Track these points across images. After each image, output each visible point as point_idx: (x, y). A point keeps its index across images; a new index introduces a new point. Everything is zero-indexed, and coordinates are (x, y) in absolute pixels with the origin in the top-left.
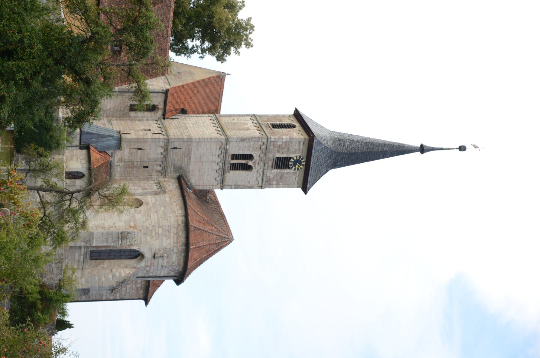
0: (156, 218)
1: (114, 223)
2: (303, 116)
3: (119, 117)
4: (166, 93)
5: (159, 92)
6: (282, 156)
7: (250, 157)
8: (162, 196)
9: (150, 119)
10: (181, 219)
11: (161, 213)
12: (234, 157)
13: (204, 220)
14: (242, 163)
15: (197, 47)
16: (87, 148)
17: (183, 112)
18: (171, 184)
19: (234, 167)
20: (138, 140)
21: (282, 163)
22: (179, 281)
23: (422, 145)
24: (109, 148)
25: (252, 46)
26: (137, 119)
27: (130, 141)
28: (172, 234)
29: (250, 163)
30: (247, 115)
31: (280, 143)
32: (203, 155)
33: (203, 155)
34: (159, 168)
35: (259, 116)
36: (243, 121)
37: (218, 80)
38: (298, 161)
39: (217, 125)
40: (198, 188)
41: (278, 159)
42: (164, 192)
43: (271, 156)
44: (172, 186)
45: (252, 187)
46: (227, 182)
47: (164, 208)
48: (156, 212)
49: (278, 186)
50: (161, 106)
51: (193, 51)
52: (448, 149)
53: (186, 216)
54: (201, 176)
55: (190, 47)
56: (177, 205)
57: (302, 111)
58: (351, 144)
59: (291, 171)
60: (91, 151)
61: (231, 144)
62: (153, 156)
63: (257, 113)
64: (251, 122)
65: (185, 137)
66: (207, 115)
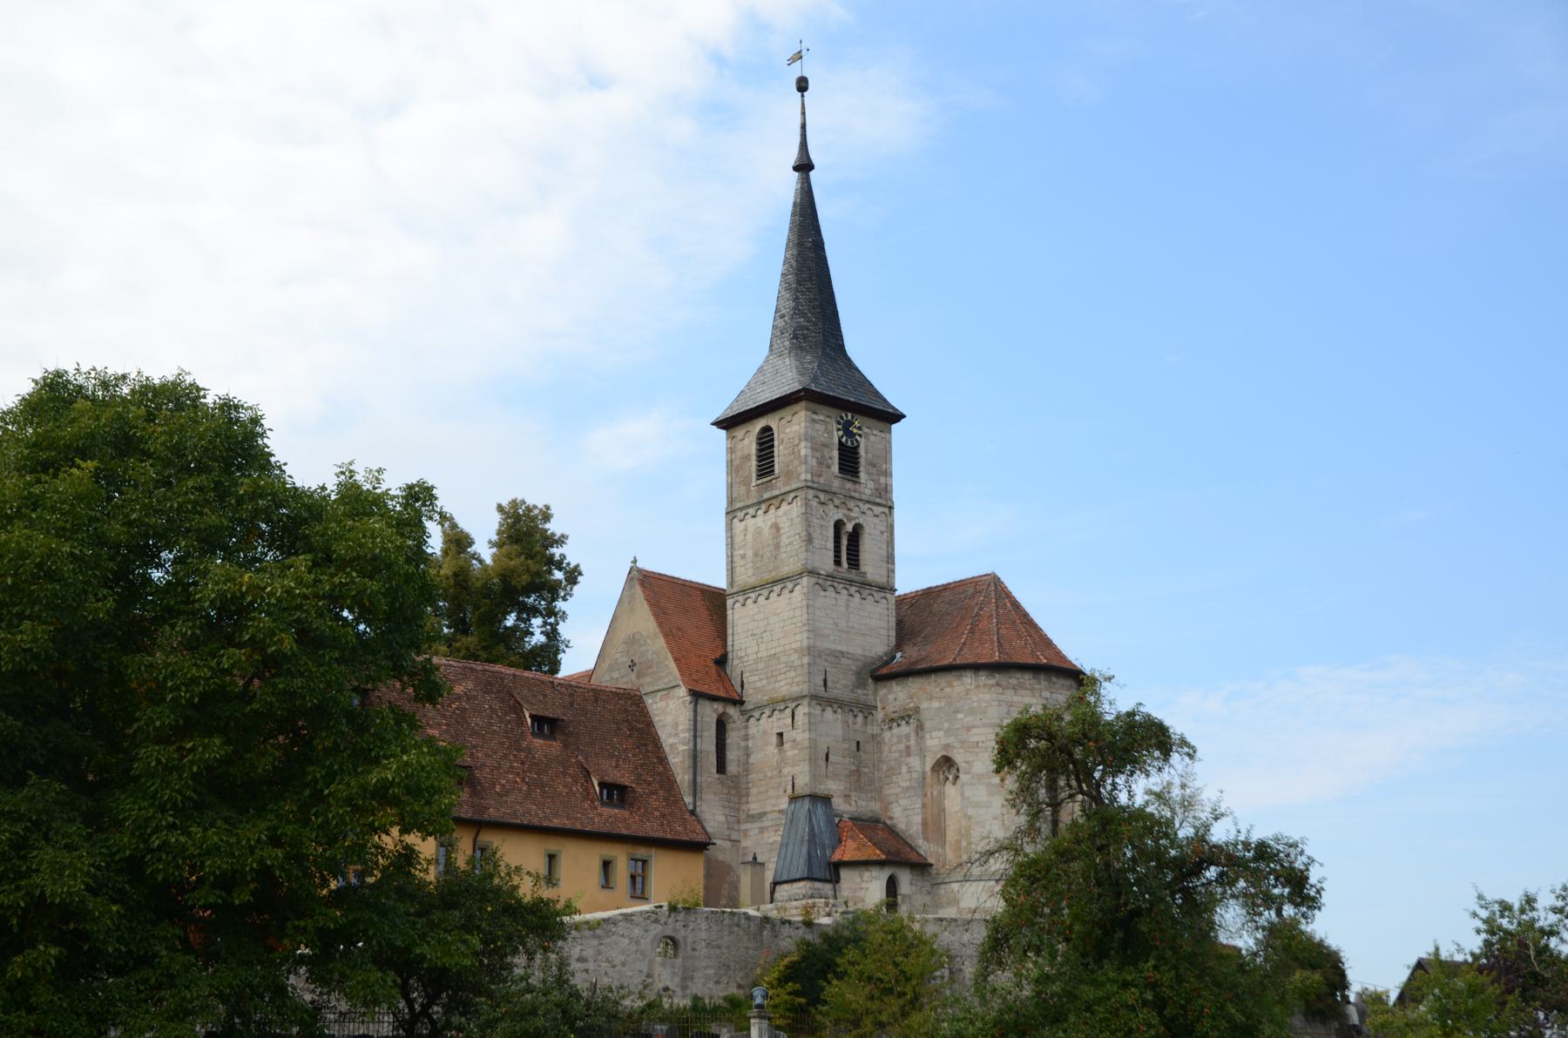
0: (982, 730)
1: (995, 818)
3: (740, 797)
4: (696, 696)
5: (695, 711)
6: (836, 460)
7: (838, 525)
8: (925, 715)
9: (743, 732)
10: (983, 678)
11: (969, 720)
12: (838, 562)
13: (972, 631)
14: (849, 544)
15: (545, 624)
16: (837, 867)
17: (722, 661)
18: (891, 697)
19: (854, 562)
20: (812, 761)
21: (849, 461)
23: (796, 169)
24: (830, 821)
25: (548, 508)
26: (743, 759)
27: (814, 777)
28: (1016, 699)
29: (849, 527)
30: (730, 528)
31: (814, 462)
32: (836, 624)
33: (836, 624)
34: (860, 718)
35: (731, 501)
36: (749, 536)
37: (651, 587)
38: (846, 428)
39: (765, 592)
40: (893, 640)
41: (841, 470)
42: (917, 710)
43: (836, 484)
44: (897, 695)
45: (891, 528)
46: (882, 580)
48: (969, 729)
49: (887, 474)
50: (719, 707)
51: (552, 635)
52: (803, 113)
53: (976, 668)
54: (870, 628)
55: (543, 639)
57: (721, 410)
58: (803, 315)
59: (863, 442)
60: (846, 858)
61: (817, 564)
62: (838, 730)
63: (722, 504)
64: (750, 521)
65: (806, 660)
66: (729, 612)
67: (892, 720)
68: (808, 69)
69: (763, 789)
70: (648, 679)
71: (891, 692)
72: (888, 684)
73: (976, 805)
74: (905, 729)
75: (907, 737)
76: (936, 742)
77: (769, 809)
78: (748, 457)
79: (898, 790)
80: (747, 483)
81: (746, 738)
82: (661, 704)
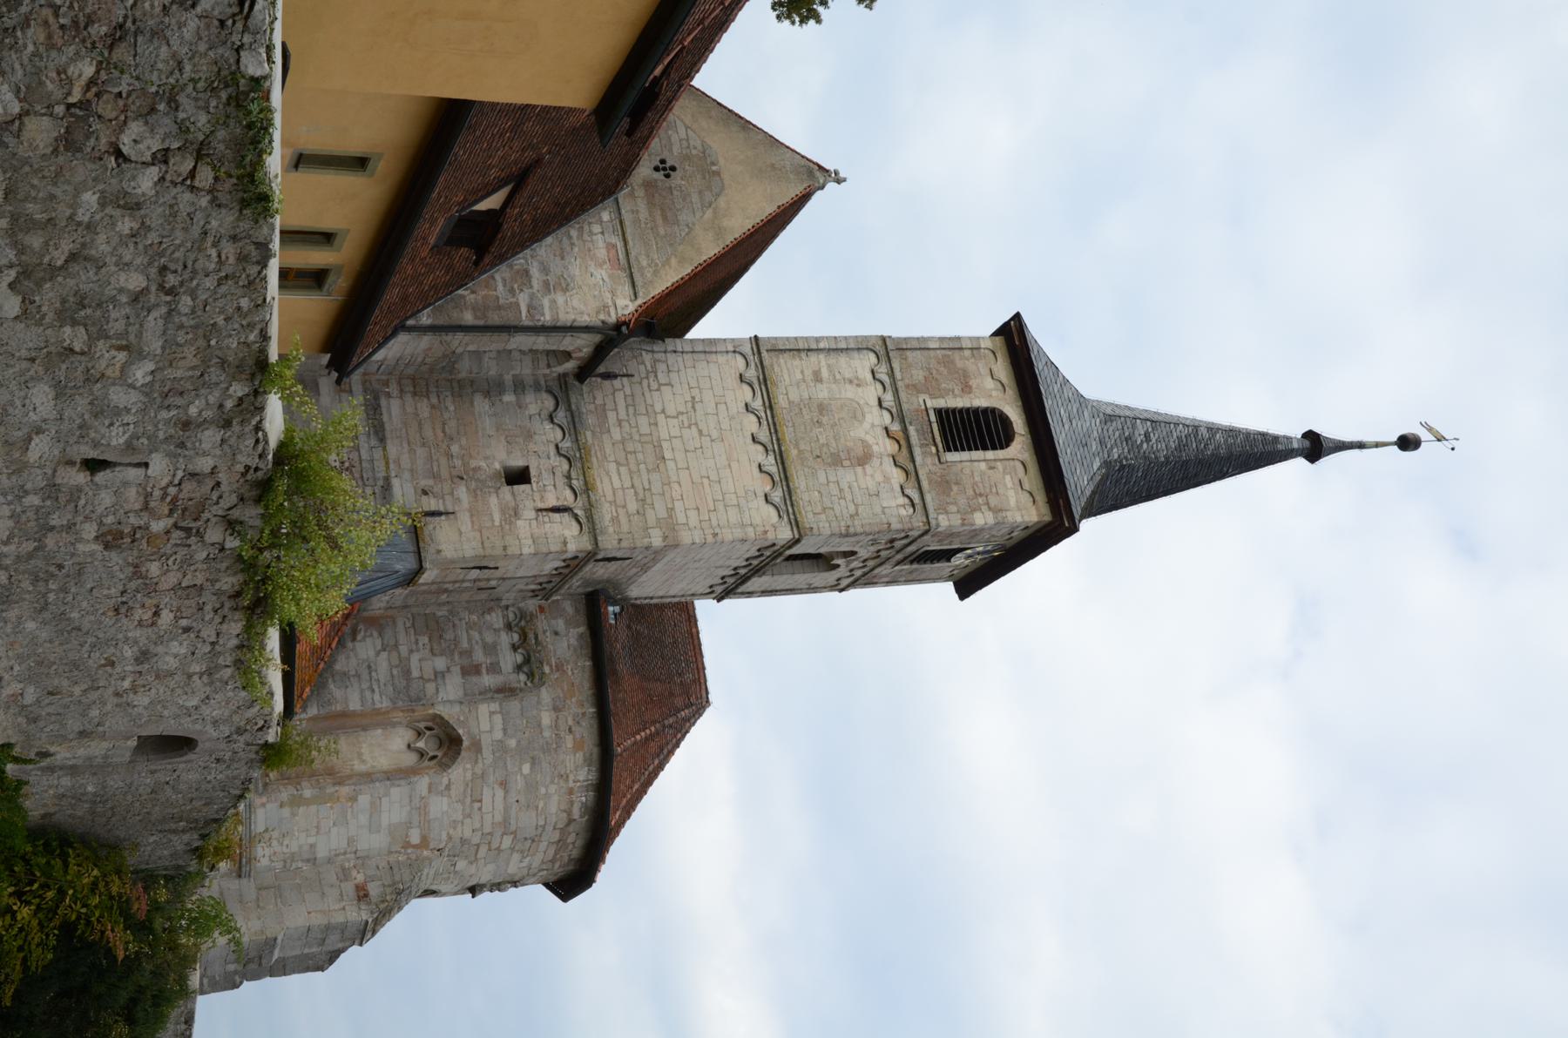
0: (499, 805)
1: (350, 841)
2: (1039, 366)
9: (529, 381)
10: (583, 798)
11: (519, 783)
18: (560, 624)
22: (572, 881)
30: (860, 346)
39: (764, 436)
47: (533, 764)
48: (504, 784)
52: (1377, 445)
57: (1044, 336)
63: (898, 328)
64: (871, 392)
68: (1428, 447)
69: (428, 433)
70: (642, 206)
71: (568, 623)
72: (582, 618)
73: (375, 808)
74: (509, 660)
75: (494, 669)
76: (485, 726)
77: (392, 450)
78: (967, 389)
79: (403, 649)
81: (519, 386)
82: (602, 253)
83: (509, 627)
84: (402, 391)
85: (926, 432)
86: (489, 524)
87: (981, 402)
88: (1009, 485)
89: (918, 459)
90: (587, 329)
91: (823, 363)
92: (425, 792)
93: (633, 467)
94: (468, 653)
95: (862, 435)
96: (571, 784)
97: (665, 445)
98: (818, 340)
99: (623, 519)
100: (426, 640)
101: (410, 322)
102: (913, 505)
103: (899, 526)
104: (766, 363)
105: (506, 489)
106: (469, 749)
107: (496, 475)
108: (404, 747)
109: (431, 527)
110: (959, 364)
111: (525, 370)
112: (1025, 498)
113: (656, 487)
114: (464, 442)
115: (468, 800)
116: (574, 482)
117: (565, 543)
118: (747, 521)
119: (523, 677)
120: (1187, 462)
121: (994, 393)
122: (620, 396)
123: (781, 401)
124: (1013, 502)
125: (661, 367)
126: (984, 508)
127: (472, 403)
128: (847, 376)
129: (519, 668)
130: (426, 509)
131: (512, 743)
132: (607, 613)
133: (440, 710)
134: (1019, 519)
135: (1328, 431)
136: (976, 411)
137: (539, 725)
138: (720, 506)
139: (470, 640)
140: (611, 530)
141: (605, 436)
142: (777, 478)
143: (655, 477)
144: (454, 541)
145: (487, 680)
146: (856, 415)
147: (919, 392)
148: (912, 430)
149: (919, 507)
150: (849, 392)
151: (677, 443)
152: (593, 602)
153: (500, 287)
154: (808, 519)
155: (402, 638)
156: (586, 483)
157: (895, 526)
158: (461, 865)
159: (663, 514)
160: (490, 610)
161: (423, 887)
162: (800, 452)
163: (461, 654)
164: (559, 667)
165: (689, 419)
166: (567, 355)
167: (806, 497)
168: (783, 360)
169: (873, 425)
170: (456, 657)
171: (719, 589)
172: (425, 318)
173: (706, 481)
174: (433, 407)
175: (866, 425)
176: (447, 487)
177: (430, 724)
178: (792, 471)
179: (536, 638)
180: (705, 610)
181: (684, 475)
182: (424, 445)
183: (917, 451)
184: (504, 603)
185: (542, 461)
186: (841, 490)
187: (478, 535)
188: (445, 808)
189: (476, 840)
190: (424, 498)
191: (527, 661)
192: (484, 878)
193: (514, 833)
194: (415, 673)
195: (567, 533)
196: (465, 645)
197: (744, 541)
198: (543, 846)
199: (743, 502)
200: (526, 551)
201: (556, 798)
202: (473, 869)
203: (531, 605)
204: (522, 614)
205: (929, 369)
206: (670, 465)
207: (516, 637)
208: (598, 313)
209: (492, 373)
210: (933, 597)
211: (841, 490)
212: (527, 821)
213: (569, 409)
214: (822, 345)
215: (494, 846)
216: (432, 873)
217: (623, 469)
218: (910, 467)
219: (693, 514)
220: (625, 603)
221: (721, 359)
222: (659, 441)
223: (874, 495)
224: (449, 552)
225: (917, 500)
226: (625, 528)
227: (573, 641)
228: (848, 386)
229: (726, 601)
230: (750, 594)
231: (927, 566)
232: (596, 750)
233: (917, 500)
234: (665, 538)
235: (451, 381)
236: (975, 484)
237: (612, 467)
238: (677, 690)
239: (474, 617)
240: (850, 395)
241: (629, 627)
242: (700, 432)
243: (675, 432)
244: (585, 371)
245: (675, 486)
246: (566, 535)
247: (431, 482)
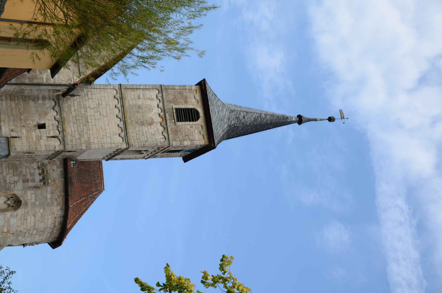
9: (47, 97)
10: (59, 220)
11: (39, 215)
18: (55, 167)
22: (56, 243)
30: (154, 87)
35: (167, 88)
39: (120, 115)
48: (34, 215)
56: (58, 204)
57: (211, 85)
64: (156, 102)
67: (43, 171)
69: (14, 112)
71: (57, 167)
72: (62, 166)
74: (38, 178)
75: (33, 181)
76: (29, 198)
78: (186, 102)
79: (4, 174)
80: (174, 101)
81: (44, 98)
83: (39, 168)
84: (6, 99)
85: (172, 116)
86: (32, 141)
87: (190, 106)
88: (196, 132)
89: (168, 124)
90: (65, 85)
91: (141, 93)
92: (9, 217)
93: (78, 124)
94: (25, 176)
95: (151, 116)
96: (55, 216)
97: (89, 118)
98: (140, 85)
99: (74, 141)
100: (12, 171)
101: (9, 82)
102: (165, 138)
103: (160, 145)
104: (123, 92)
105: (38, 130)
106: (24, 204)
107: (35, 126)
108: (3, 203)
109: (13, 141)
110: (185, 94)
111: (46, 94)
112: (201, 137)
113: (85, 131)
114: (25, 115)
115: (23, 219)
116: (59, 129)
117: (55, 147)
118: (113, 142)
119: (42, 183)
120: (256, 125)
121: (195, 104)
122: (76, 102)
123: (126, 105)
124: (197, 138)
125: (90, 93)
126: (188, 140)
127: (29, 103)
128: (148, 97)
129: (41, 181)
130: (12, 136)
131: (38, 203)
132: (71, 164)
133: (15, 192)
134: (198, 143)
135: (305, 115)
136: (188, 109)
137: (47, 198)
138: (105, 137)
139: (26, 172)
140: (70, 144)
141: (70, 115)
142: (123, 129)
143: (85, 128)
144: (19, 146)
145: (31, 184)
146: (150, 109)
147: (171, 103)
148: (167, 115)
149: (167, 139)
150: (149, 102)
151: (93, 117)
152: (65, 162)
153: (38, 72)
154: (132, 141)
155: (4, 170)
156: (63, 129)
157: (159, 144)
158: (20, 238)
159: (86, 139)
160: (33, 162)
161: (7, 244)
162: (131, 121)
163: (23, 176)
164: (54, 181)
165: (97, 110)
166: (59, 91)
167: (132, 135)
168: (128, 92)
169: (155, 113)
170: (21, 177)
171: (106, 158)
172: (13, 81)
173: (101, 129)
174: (16, 104)
175: (153, 113)
176: (19, 129)
177: (12, 196)
178: (129, 126)
179: (47, 172)
180: (104, 162)
181: (94, 127)
182: (12, 116)
183: (168, 121)
184: (37, 161)
185: (50, 122)
186: (143, 133)
187: (28, 144)
188: (15, 221)
189: (25, 231)
190: (12, 132)
191: (44, 178)
192: (28, 241)
193: (37, 229)
194: (8, 181)
195: (56, 144)
196: (24, 173)
197: (111, 148)
198: (46, 233)
199: (112, 136)
200: (43, 149)
201: (50, 220)
202: (23, 239)
203: (46, 162)
204: (43, 164)
205: (175, 96)
206: (90, 124)
207: (41, 171)
208: (68, 81)
209: (36, 94)
210: (177, 161)
211: (143, 133)
212: (41, 226)
213: (59, 106)
214: (141, 87)
215: (30, 233)
216: (11, 240)
217: (75, 125)
218: (166, 127)
219: (96, 139)
220: (77, 161)
221: (109, 91)
222: (87, 116)
223: (154, 135)
224: (18, 149)
225: (167, 137)
226: (74, 143)
227: (59, 173)
228: (148, 100)
229: (109, 161)
230: (116, 159)
231: (172, 154)
232: (64, 206)
233: (167, 137)
234: (87, 147)
235: (22, 96)
236: (186, 132)
237: (72, 124)
238: (93, 186)
239: (28, 165)
240: (149, 103)
241: (78, 167)
242: (100, 114)
243: (92, 114)
244: (65, 95)
245: (91, 131)
246: (56, 145)
247: (14, 127)
